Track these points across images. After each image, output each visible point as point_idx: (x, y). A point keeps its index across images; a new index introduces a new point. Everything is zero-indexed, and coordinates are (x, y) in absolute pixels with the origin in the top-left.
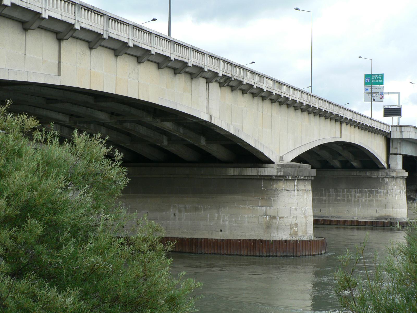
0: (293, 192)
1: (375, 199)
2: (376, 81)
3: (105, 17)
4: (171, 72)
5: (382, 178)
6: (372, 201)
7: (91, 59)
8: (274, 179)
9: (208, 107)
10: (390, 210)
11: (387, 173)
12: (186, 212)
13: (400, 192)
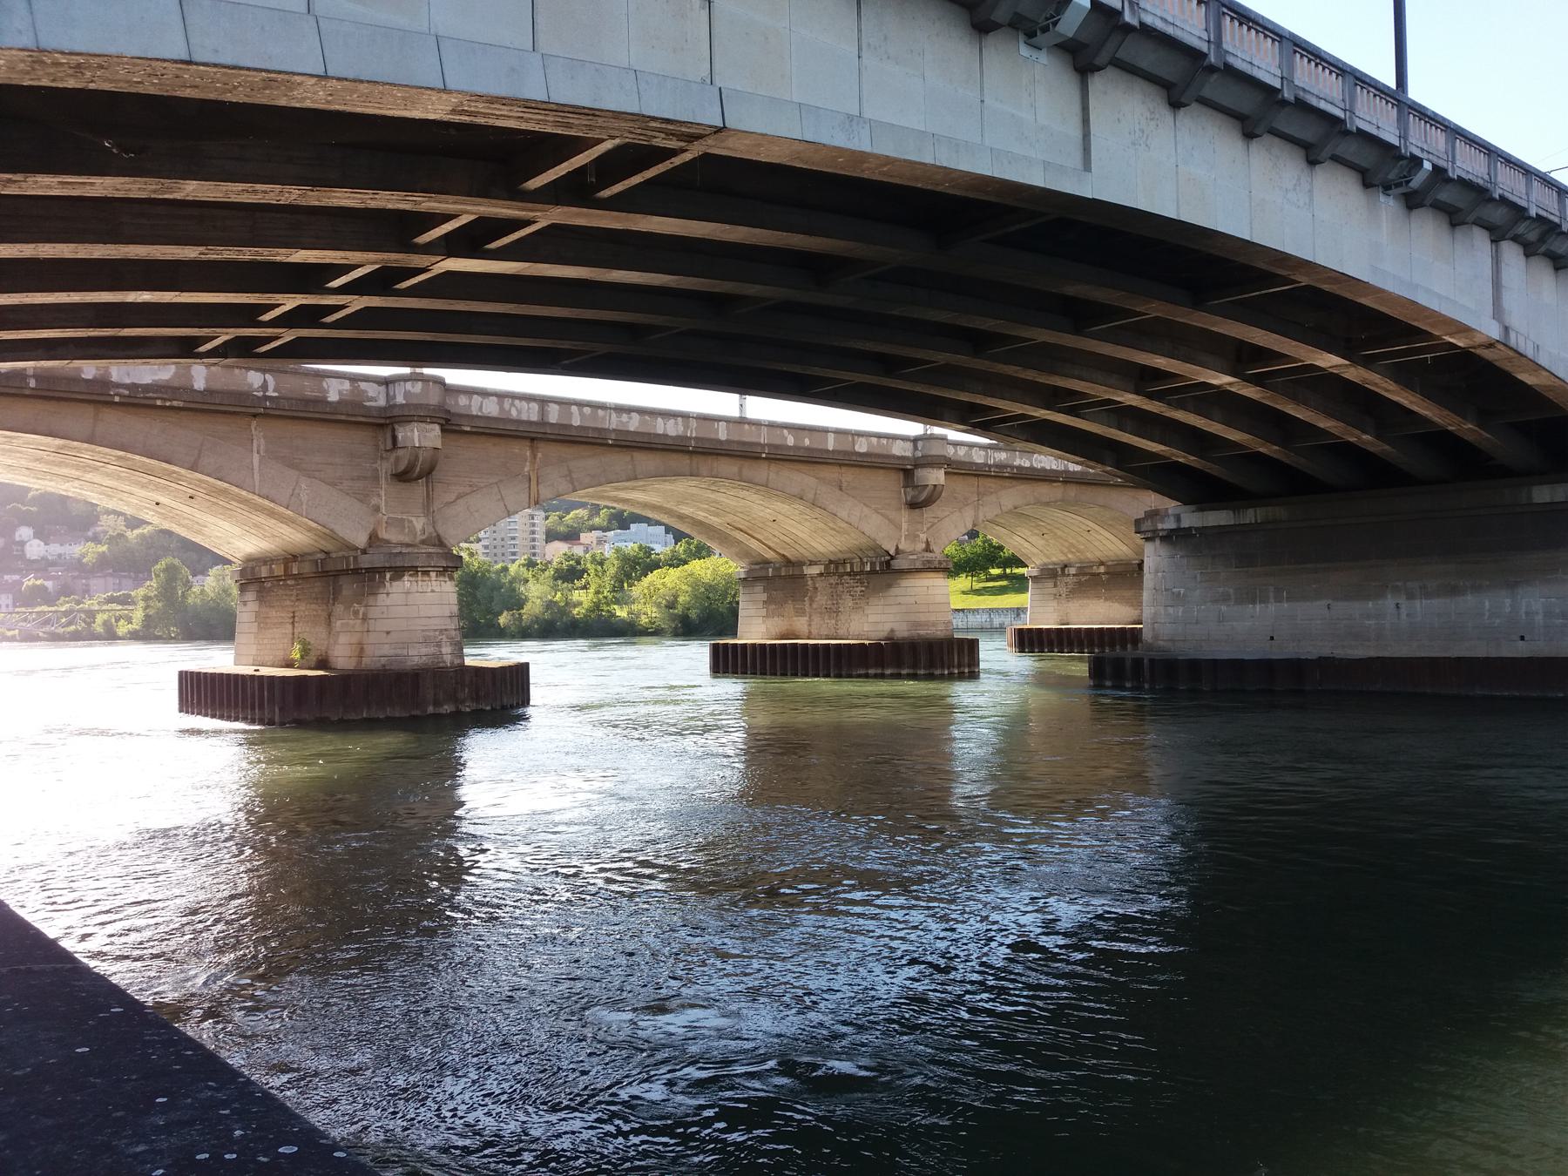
7: (1175, 137)
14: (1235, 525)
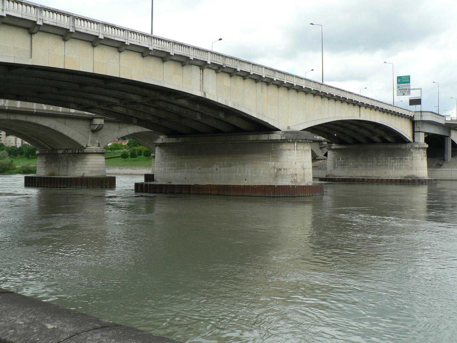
0: (293, 151)
1: (404, 164)
2: (405, 81)
3: (71, 17)
4: (286, 89)
5: (409, 149)
6: (402, 165)
8: (280, 142)
9: (203, 87)
10: (414, 171)
11: (412, 145)
12: (224, 167)
13: (422, 159)
14: (177, 143)
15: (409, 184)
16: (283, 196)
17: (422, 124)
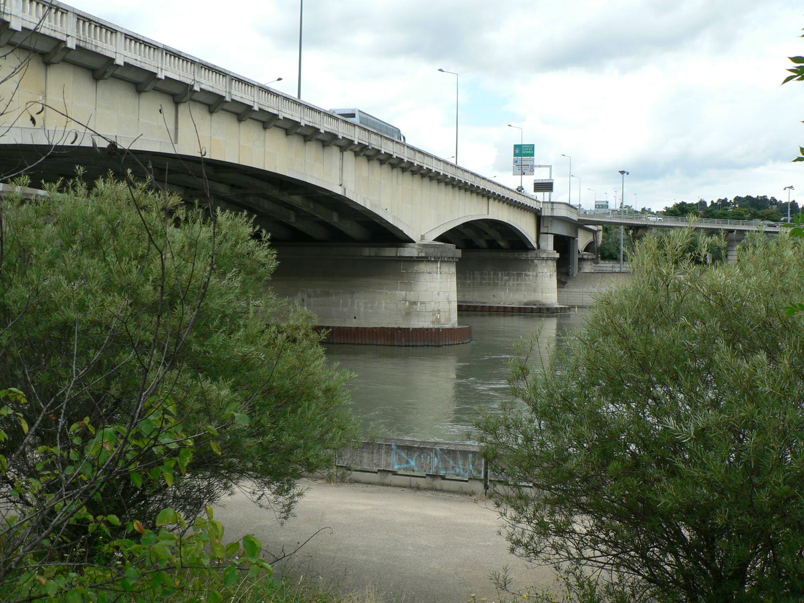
5: (532, 260)
11: (537, 254)
13: (551, 275)
15: (532, 316)
16: (422, 344)
17: (551, 221)
